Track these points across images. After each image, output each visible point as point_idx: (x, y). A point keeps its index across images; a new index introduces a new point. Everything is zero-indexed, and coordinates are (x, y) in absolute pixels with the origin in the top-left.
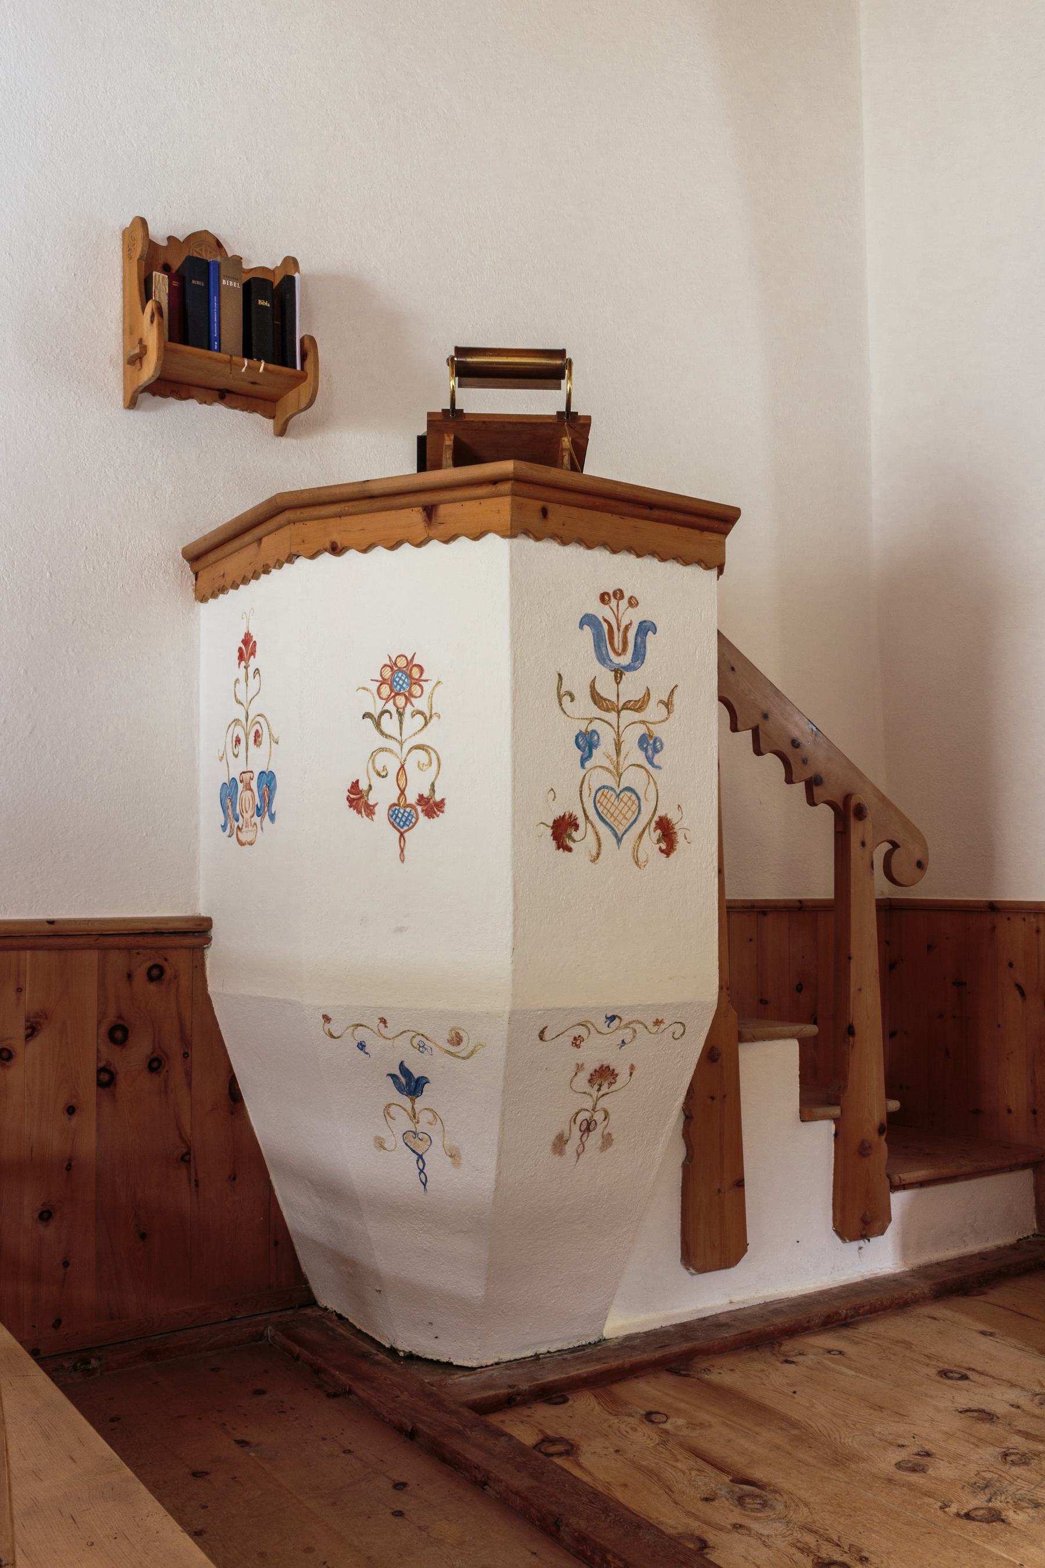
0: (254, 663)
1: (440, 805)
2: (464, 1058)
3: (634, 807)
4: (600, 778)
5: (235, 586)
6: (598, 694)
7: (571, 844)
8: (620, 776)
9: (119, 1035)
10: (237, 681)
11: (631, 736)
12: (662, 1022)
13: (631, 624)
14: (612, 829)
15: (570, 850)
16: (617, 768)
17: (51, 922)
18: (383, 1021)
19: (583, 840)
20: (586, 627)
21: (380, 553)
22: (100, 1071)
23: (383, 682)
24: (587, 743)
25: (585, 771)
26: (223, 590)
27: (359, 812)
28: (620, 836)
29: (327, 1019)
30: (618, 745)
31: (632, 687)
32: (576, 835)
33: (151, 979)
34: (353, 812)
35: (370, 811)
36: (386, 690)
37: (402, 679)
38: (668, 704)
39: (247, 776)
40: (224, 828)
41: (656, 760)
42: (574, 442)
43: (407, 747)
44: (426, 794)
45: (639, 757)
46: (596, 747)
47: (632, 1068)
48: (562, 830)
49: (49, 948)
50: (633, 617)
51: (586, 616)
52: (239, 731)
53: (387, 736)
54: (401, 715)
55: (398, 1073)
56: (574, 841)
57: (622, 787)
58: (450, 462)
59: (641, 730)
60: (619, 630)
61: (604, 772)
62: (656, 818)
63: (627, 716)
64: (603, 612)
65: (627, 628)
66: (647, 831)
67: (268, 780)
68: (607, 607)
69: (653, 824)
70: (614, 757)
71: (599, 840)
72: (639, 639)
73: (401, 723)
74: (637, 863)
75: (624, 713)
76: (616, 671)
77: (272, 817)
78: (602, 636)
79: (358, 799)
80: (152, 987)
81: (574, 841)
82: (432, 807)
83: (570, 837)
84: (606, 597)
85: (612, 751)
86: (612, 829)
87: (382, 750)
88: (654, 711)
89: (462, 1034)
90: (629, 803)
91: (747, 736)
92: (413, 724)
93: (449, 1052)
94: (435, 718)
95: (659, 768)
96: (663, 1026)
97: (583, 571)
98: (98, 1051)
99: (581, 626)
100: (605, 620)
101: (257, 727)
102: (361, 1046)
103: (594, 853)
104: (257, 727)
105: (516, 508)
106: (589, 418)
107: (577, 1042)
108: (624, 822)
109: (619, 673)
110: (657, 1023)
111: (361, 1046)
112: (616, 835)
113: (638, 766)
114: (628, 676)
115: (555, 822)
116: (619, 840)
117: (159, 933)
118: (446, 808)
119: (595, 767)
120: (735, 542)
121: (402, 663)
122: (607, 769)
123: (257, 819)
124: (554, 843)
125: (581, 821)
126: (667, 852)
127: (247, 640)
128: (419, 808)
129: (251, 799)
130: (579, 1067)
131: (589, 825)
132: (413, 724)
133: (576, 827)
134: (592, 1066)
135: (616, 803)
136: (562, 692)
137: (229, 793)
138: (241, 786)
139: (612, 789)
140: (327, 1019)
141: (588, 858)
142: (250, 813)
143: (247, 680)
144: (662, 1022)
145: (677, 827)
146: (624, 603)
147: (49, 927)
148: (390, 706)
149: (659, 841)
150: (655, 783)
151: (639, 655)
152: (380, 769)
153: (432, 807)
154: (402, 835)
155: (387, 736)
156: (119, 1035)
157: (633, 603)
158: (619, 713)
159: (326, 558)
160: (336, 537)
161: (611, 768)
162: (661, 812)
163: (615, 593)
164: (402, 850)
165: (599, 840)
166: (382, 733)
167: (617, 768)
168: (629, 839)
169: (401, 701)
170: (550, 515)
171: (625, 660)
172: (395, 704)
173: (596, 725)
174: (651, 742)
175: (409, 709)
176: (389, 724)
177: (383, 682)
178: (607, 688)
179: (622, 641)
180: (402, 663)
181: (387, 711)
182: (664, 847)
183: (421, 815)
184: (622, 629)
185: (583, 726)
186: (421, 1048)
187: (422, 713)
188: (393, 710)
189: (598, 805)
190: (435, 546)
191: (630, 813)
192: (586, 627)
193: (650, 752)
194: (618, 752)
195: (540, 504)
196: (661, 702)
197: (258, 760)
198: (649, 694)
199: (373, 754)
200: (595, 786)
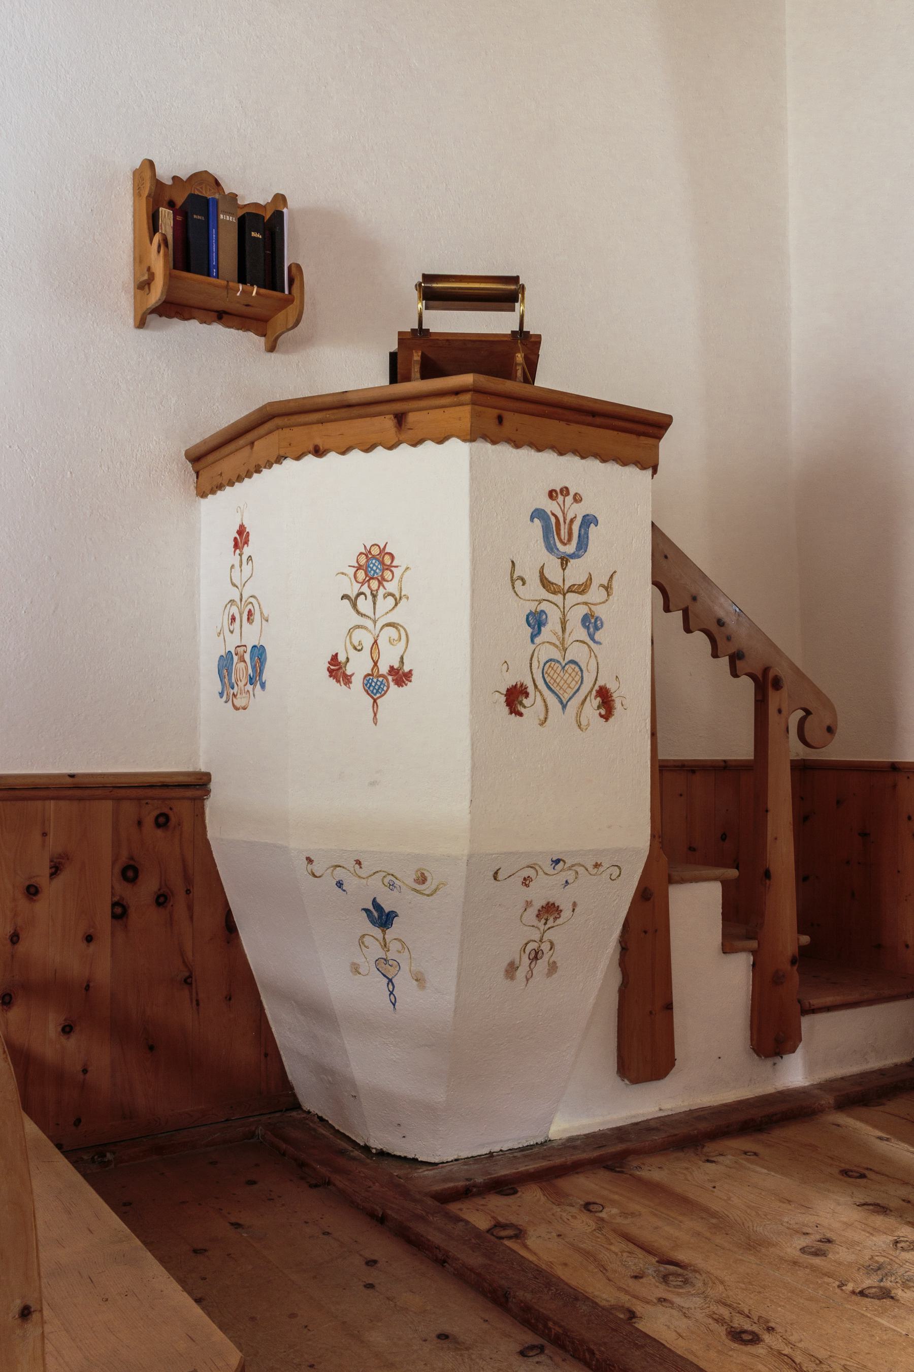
0: (247, 551)
1: (408, 676)
3: (578, 678)
4: (546, 652)
6: (546, 579)
8: (565, 650)
9: (130, 874)
10: (233, 566)
11: (575, 616)
12: (600, 865)
14: (558, 697)
15: (521, 714)
16: (563, 643)
17: (72, 776)
19: (532, 706)
20: (536, 520)
22: (114, 905)
23: (359, 567)
24: (536, 621)
25: (533, 647)
26: (220, 487)
27: (338, 681)
29: (310, 860)
30: (564, 623)
31: (576, 573)
33: (158, 825)
36: (361, 575)
37: (375, 565)
38: (608, 588)
39: (241, 650)
41: (597, 637)
42: (526, 358)
43: (379, 624)
45: (582, 634)
46: (544, 625)
48: (515, 697)
49: (70, 798)
50: (577, 511)
51: (536, 510)
52: (234, 610)
53: (362, 615)
54: (374, 596)
55: (371, 908)
56: (525, 707)
58: (418, 375)
59: (584, 610)
62: (597, 688)
63: (572, 598)
64: (551, 507)
65: (572, 521)
67: (259, 653)
68: (555, 502)
69: (594, 693)
70: (560, 633)
72: (583, 531)
73: (374, 604)
74: (579, 726)
76: (562, 559)
77: (263, 686)
78: (551, 528)
79: (337, 670)
80: (159, 833)
81: (525, 707)
82: (401, 677)
83: (521, 703)
84: (554, 494)
86: (558, 697)
87: (358, 627)
88: (595, 594)
89: (426, 874)
90: (573, 674)
91: (678, 616)
92: (385, 604)
95: (600, 643)
96: (601, 869)
97: (534, 472)
99: (532, 519)
100: (553, 514)
101: (250, 606)
102: (340, 884)
105: (475, 415)
107: (526, 882)
108: (569, 690)
109: (564, 560)
112: (561, 702)
115: (508, 690)
116: (564, 706)
119: (544, 643)
120: (667, 446)
122: (554, 645)
123: (249, 687)
125: (531, 689)
127: (241, 531)
128: (390, 678)
130: (529, 904)
131: (538, 693)
132: (385, 604)
133: (527, 695)
134: (538, 904)
135: (562, 674)
136: (515, 577)
137: (225, 664)
138: (236, 658)
139: (558, 662)
140: (310, 860)
142: (244, 682)
144: (600, 865)
145: (615, 695)
146: (569, 499)
148: (365, 589)
149: (599, 707)
150: (596, 657)
151: (583, 544)
152: (356, 644)
153: (401, 677)
154: (375, 701)
155: (362, 615)
156: (130, 874)
157: (577, 499)
158: (564, 595)
159: (310, 459)
160: (319, 441)
161: (558, 643)
163: (561, 490)
166: (358, 612)
167: (563, 643)
169: (374, 584)
170: (505, 422)
171: (571, 549)
172: (369, 587)
173: (544, 606)
174: (593, 621)
175: (381, 591)
176: (364, 605)
178: (554, 574)
179: (564, 530)
180: (375, 551)
181: (363, 593)
182: (603, 712)
183: (392, 684)
184: (568, 521)
185: (532, 606)
186: (392, 886)
187: (393, 595)
188: (368, 592)
189: (546, 676)
190: (404, 450)
191: (574, 683)
192: (536, 520)
193: (592, 630)
194: (564, 630)
195: (496, 412)
196: (602, 586)
197: (251, 636)
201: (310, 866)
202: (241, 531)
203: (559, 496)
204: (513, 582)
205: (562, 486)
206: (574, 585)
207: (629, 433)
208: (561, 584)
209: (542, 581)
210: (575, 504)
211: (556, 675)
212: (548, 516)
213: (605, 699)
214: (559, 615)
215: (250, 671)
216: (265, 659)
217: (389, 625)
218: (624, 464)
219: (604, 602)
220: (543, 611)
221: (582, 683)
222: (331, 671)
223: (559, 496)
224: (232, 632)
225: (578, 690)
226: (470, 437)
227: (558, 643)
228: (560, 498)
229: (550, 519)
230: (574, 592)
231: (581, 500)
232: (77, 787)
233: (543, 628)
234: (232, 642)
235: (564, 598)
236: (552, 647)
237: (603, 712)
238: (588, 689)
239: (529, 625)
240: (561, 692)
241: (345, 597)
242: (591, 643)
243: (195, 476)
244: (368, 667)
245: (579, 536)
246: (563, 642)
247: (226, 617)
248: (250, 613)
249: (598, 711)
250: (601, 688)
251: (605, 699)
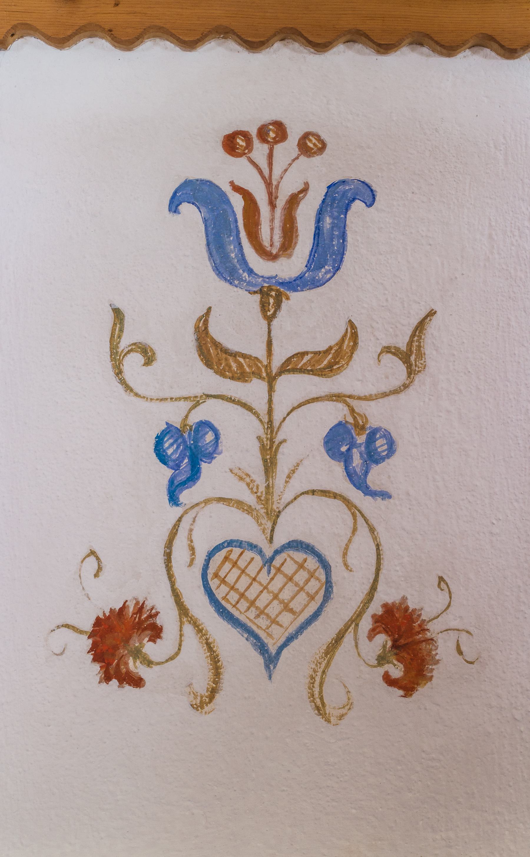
4: (212, 526)
6: (216, 344)
8: (275, 517)
11: (305, 434)
13: (305, 190)
15: (137, 682)
19: (171, 663)
20: (186, 208)
24: (185, 452)
25: (178, 511)
28: (273, 650)
31: (308, 322)
38: (410, 356)
45: (333, 475)
46: (210, 457)
48: (117, 642)
51: (187, 183)
56: (149, 663)
57: (280, 539)
59: (332, 414)
60: (272, 205)
61: (174, 563)
63: (293, 388)
64: (228, 172)
65: (294, 201)
66: (349, 637)
68: (243, 160)
69: (366, 624)
70: (259, 478)
71: (209, 646)
72: (328, 221)
74: (320, 709)
78: (227, 225)
81: (149, 663)
83: (137, 654)
84: (241, 142)
85: (254, 463)
88: (363, 375)
90: (301, 577)
95: (385, 495)
99: (174, 206)
100: (237, 189)
103: (202, 686)
108: (286, 618)
109: (271, 297)
112: (262, 648)
113: (325, 493)
115: (98, 622)
116: (271, 660)
119: (207, 501)
122: (240, 504)
124: (97, 667)
125: (168, 618)
126: (407, 686)
131: (188, 629)
133: (156, 633)
135: (263, 577)
139: (252, 547)
141: (183, 704)
145: (434, 628)
146: (286, 150)
149: (381, 660)
150: (372, 530)
151: (329, 253)
158: (271, 380)
161: (250, 499)
162: (387, 595)
163: (262, 133)
165: (209, 646)
168: (298, 660)
174: (361, 439)
178: (238, 323)
182: (397, 671)
184: (281, 203)
185: (174, 413)
189: (213, 584)
191: (302, 598)
192: (186, 208)
193: (357, 461)
194: (269, 465)
198: (355, 336)
203: (256, 142)
205: (268, 117)
206: (303, 354)
208: (260, 352)
210: (303, 158)
211: (244, 582)
212: (223, 195)
218: (448, 48)
219: (396, 392)
221: (327, 597)
223: (256, 142)
225: (316, 615)
227: (250, 499)
228: (260, 151)
229: (227, 202)
230: (302, 371)
231: (324, 146)
233: (204, 466)
235: (271, 389)
237: (397, 671)
238: (348, 613)
239: (162, 458)
240: (263, 622)
242: (355, 495)
245: (318, 233)
246: (266, 497)
249: (381, 671)
250: (389, 610)
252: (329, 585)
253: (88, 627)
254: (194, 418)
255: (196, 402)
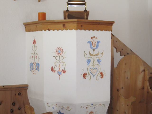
0: (36, 45)
1: (65, 71)
2: (96, 68)
3: (96, 71)
5: (32, 31)
7: (86, 78)
8: (94, 66)
9: (14, 104)
10: (33, 47)
11: (96, 60)
12: (101, 105)
13: (96, 42)
14: (93, 75)
15: (86, 78)
16: (94, 65)
17: (3, 86)
18: (57, 104)
19: (88, 77)
20: (89, 43)
21: (56, 31)
22: (11, 110)
23: (57, 51)
24: (89, 61)
26: (30, 31)
27: (53, 72)
29: (48, 104)
30: (94, 61)
31: (96, 52)
32: (87, 76)
33: (19, 95)
34: (52, 72)
35: (55, 71)
36: (57, 53)
37: (60, 51)
38: (102, 54)
39: (34, 63)
40: (30, 70)
41: (100, 63)
42: (87, 14)
43: (60, 62)
44: (63, 69)
45: (97, 63)
47: (96, 112)
48: (84, 75)
49: (3, 91)
50: (96, 40)
51: (89, 41)
52: (33, 55)
53: (57, 60)
54: (59, 57)
55: (59, 112)
57: (94, 68)
58: (67, 19)
59: (98, 58)
62: (100, 72)
63: (95, 56)
65: (95, 42)
67: (38, 65)
69: (100, 73)
71: (90, 76)
73: (59, 58)
74: (97, 80)
75: (95, 56)
76: (93, 49)
77: (39, 71)
78: (91, 44)
79: (52, 69)
80: (19, 96)
82: (64, 72)
83: (86, 76)
86: (93, 75)
87: (56, 62)
88: (100, 55)
89: (69, 107)
91: (119, 53)
92: (61, 58)
93: (67, 110)
94: (65, 58)
96: (101, 105)
97: (88, 34)
98: (11, 107)
99: (88, 43)
100: (92, 42)
101: (36, 55)
102: (53, 108)
104: (36, 55)
105: (78, 26)
106: (89, 11)
107: (87, 108)
108: (95, 73)
109: (94, 50)
110: (100, 105)
111: (53, 108)
112: (93, 75)
114: (96, 50)
116: (94, 76)
117: (20, 87)
118: (66, 72)
120: (114, 26)
121: (60, 49)
122: (92, 65)
123: (36, 70)
125: (88, 74)
126: (102, 78)
127: (34, 41)
128: (62, 72)
129: (35, 67)
130: (87, 112)
132: (61, 58)
133: (87, 75)
134: (89, 112)
136: (85, 53)
137: (31, 65)
138: (33, 64)
140: (48, 104)
142: (35, 69)
143: (34, 47)
144: (101, 105)
146: (95, 38)
147: (3, 87)
148: (58, 55)
149: (100, 76)
151: (97, 46)
152: (56, 65)
153: (64, 72)
154: (59, 75)
155: (57, 60)
156: (14, 104)
157: (96, 38)
158: (94, 56)
159: (47, 31)
160: (49, 28)
161: (92, 65)
162: (101, 71)
163: (93, 37)
164: (60, 78)
165: (90, 76)
166: (56, 59)
167: (94, 65)
169: (59, 55)
170: (83, 26)
171: (95, 47)
172: (58, 55)
173: (90, 58)
175: (61, 56)
176: (58, 58)
177: (57, 51)
178: (92, 52)
179: (94, 45)
180: (60, 49)
181: (57, 56)
182: (101, 77)
183: (62, 73)
184: (95, 42)
185: (88, 59)
186: (62, 109)
187: (62, 57)
188: (58, 56)
190: (64, 30)
192: (89, 43)
193: (99, 62)
194: (94, 62)
195: (81, 25)
196: (101, 54)
197: (36, 61)
199: (55, 63)
200: (90, 68)
201: (48, 105)
202: (34, 41)
204: (84, 54)
207: (106, 25)
209: (90, 54)
213: (102, 74)
214: (93, 60)
215: (36, 67)
216: (39, 66)
217: (62, 62)
220: (90, 59)
222: (51, 70)
224: (33, 59)
226: (77, 29)
228: (93, 38)
232: (4, 88)
234: (33, 61)
236: (92, 66)
237: (101, 77)
239: (87, 62)
241: (54, 56)
243: (25, 27)
244: (58, 69)
247: (31, 56)
248: (36, 57)
250: (101, 72)
251: (102, 74)
252: (97, 71)
253: (83, 75)
254: (89, 59)
255: (89, 58)
